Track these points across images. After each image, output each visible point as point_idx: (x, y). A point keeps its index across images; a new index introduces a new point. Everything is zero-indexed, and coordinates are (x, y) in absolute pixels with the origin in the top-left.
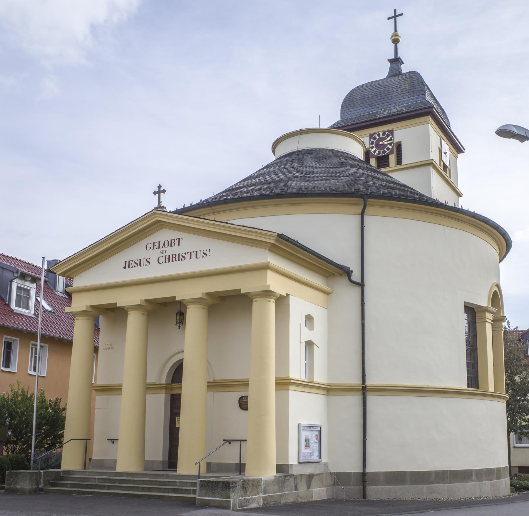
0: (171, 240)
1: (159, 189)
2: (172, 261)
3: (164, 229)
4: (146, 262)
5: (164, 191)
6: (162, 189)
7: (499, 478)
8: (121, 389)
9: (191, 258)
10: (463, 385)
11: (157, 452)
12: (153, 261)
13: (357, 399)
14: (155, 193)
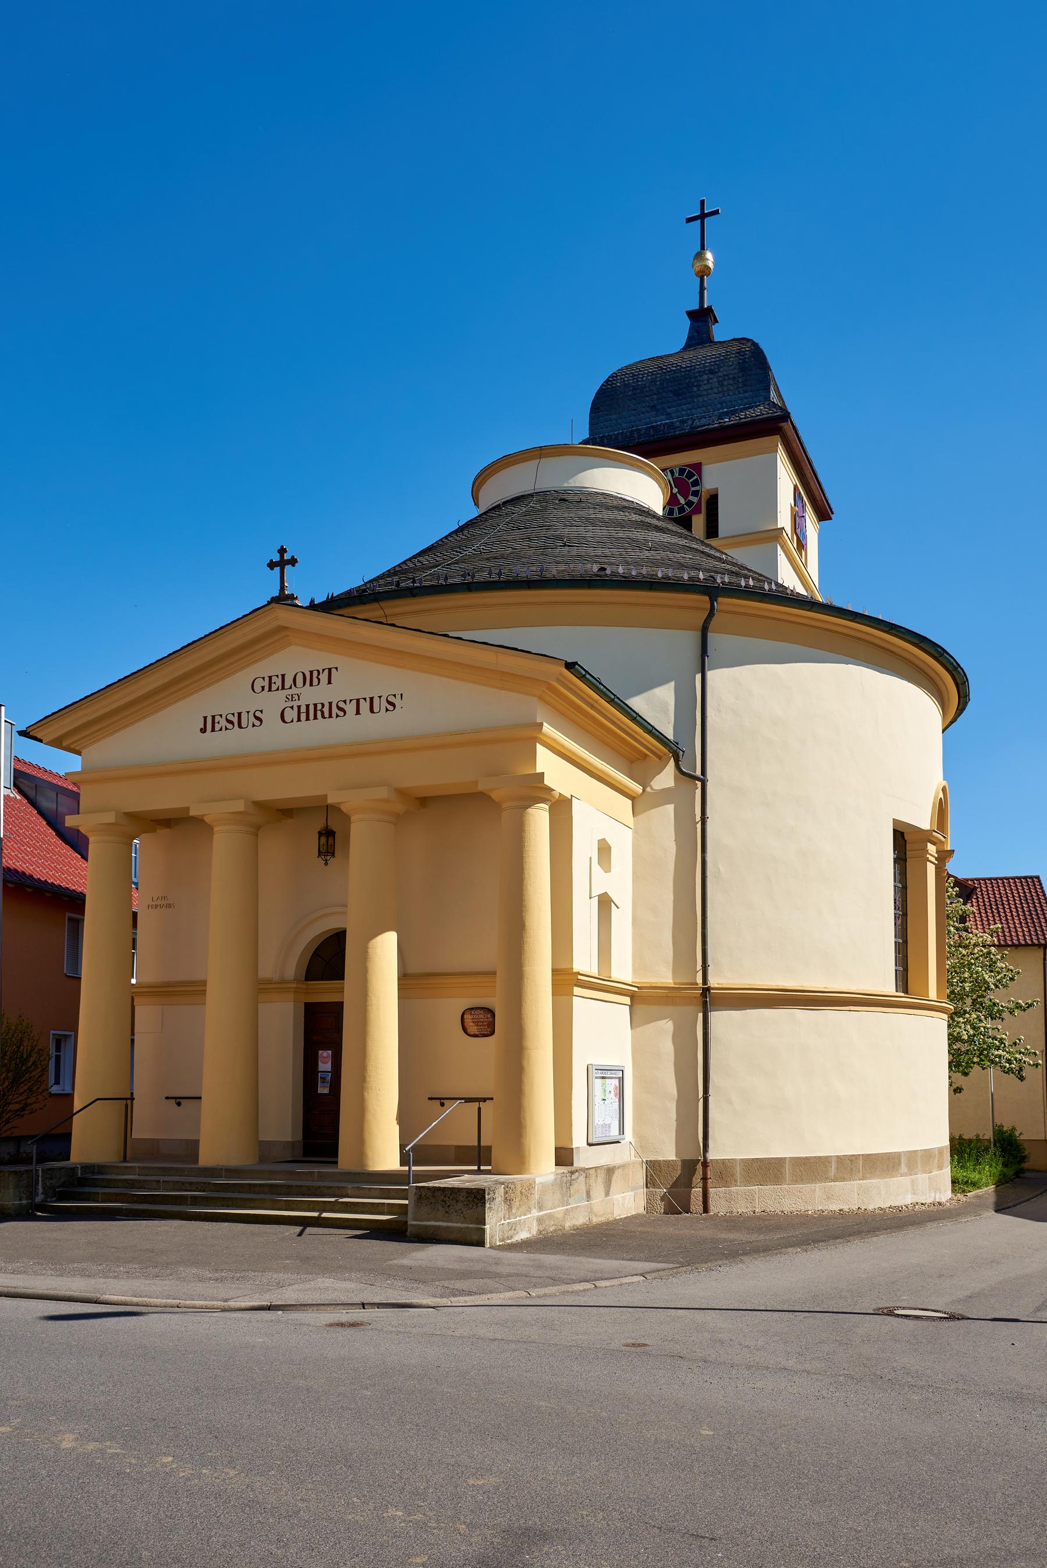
0: (311, 672)
1: (282, 556)
2: (315, 718)
3: (293, 648)
4: (252, 719)
5: (293, 561)
6: (287, 557)
7: (911, 1170)
8: (204, 992)
9: (358, 713)
10: (886, 984)
11: (282, 1123)
12: (271, 717)
13: (724, 603)
14: (272, 565)
